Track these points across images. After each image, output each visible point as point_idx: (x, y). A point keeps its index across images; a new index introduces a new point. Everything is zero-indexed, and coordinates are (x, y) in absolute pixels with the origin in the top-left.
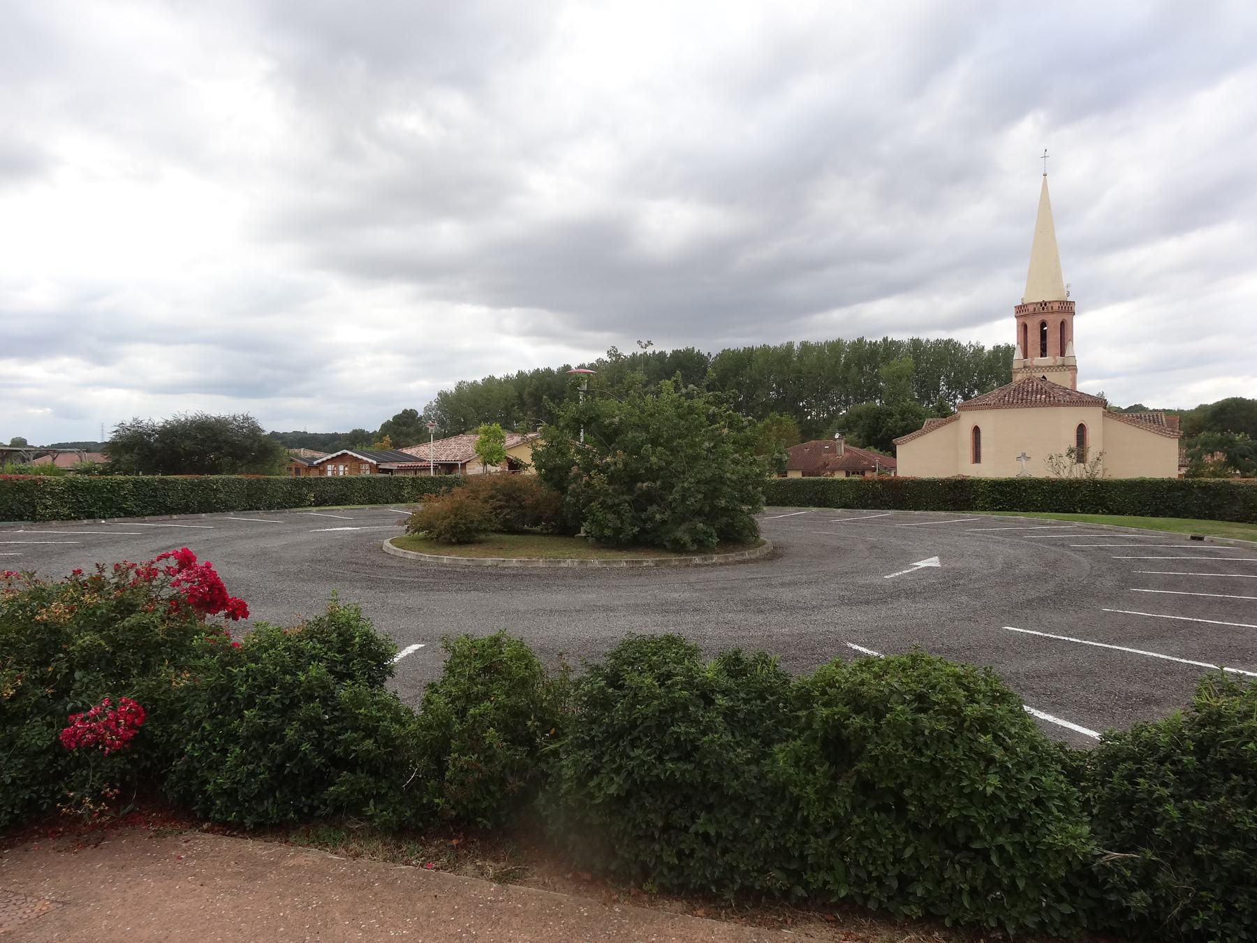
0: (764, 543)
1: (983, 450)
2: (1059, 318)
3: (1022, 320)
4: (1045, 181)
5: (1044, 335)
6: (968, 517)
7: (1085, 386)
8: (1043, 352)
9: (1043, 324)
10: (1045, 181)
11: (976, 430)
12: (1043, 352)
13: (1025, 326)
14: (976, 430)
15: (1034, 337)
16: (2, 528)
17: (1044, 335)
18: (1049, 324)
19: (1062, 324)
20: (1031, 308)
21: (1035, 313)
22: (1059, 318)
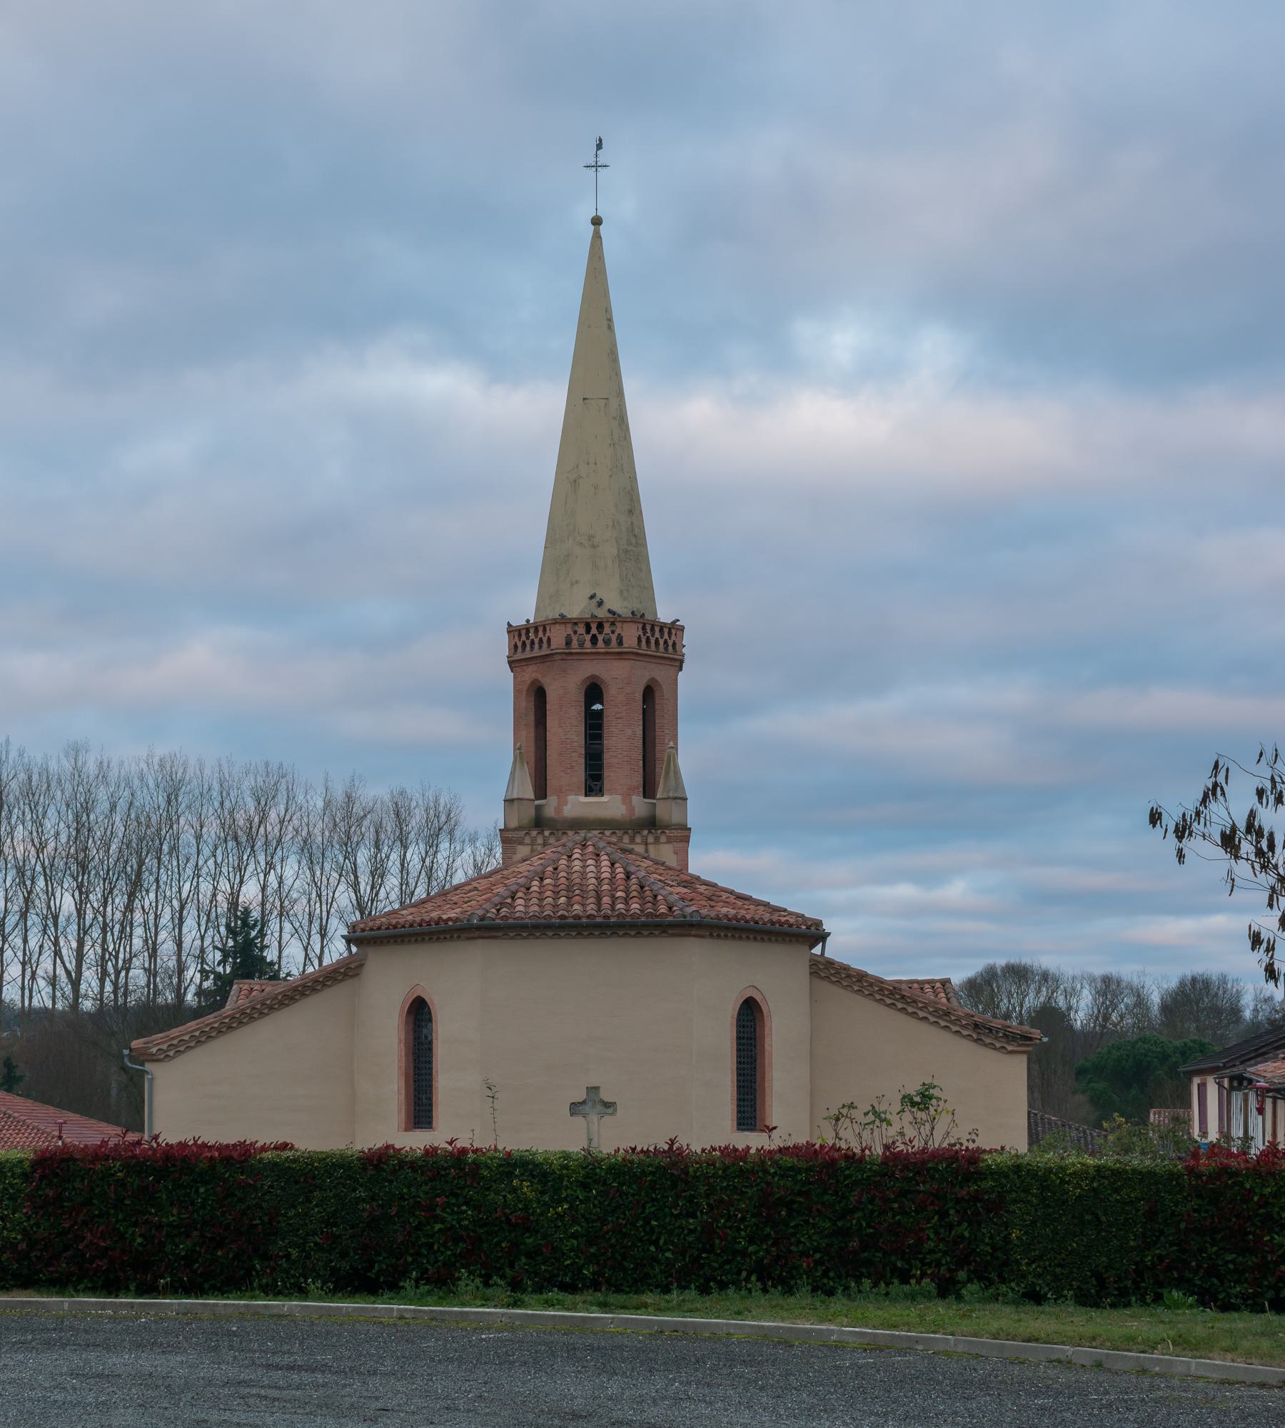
0: (21, 1078)
1: (445, 1081)
2: (642, 674)
3: (531, 673)
4: (597, 237)
5: (594, 726)
6: (387, 1308)
7: (720, 860)
8: (594, 784)
9: (594, 692)
10: (597, 237)
11: (419, 1012)
12: (594, 784)
13: (539, 695)
14: (419, 1012)
15: (566, 729)
16: (1284, 1076)
17: (594, 726)
18: (611, 692)
19: (649, 693)
20: (558, 636)
21: (568, 654)
22: (642, 674)
